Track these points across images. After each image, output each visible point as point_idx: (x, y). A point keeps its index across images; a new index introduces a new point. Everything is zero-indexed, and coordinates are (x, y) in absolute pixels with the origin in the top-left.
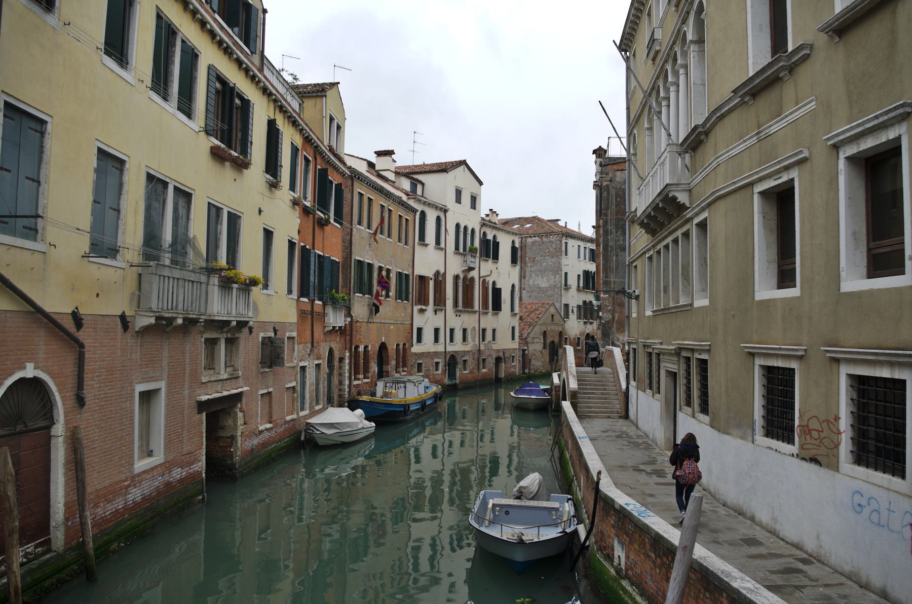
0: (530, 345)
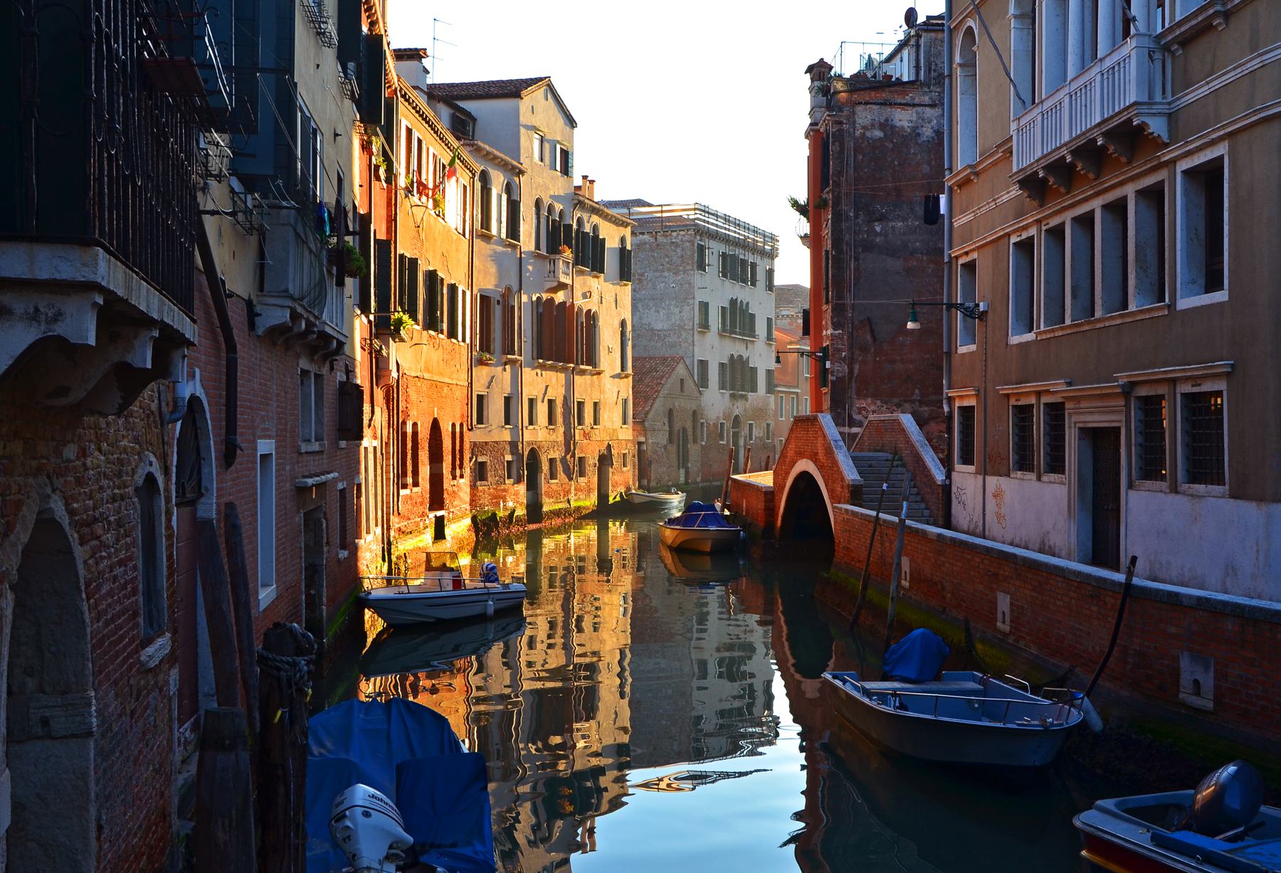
0: (649, 434)
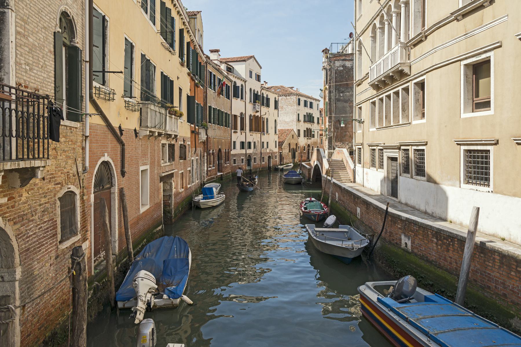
0: (283, 150)
